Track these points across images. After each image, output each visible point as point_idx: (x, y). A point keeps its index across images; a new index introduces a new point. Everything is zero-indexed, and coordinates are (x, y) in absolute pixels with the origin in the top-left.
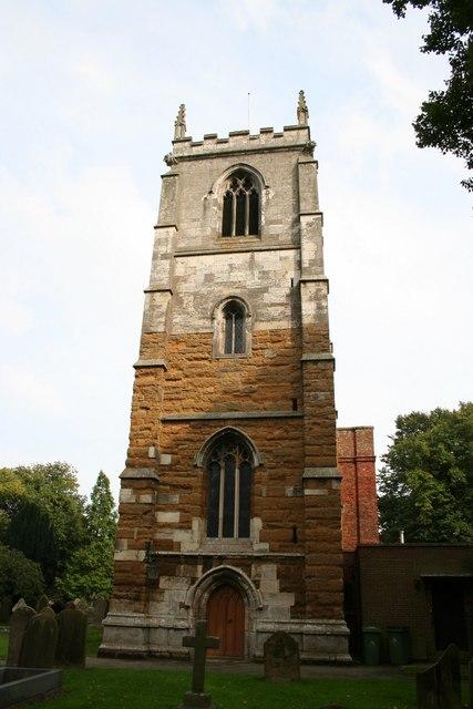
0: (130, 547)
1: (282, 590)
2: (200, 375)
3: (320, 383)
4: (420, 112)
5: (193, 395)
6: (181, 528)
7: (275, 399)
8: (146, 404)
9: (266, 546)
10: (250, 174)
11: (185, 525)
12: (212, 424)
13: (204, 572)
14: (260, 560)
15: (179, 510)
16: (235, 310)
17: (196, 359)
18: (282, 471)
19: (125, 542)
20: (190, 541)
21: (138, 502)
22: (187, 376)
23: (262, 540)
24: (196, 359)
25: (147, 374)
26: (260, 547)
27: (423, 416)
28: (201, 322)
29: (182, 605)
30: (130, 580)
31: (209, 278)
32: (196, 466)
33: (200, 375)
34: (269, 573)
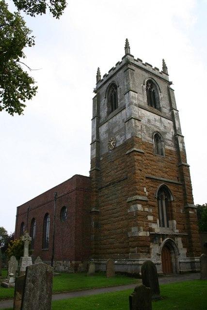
0: (144, 230)
1: (183, 247)
2: (151, 160)
3: (187, 174)
4: (27, 102)
5: (150, 168)
6: (154, 223)
7: (173, 176)
8: (140, 168)
9: (178, 231)
10: (154, 84)
11: (154, 222)
12: (158, 181)
13: (163, 240)
14: (177, 236)
15: (153, 215)
16: (158, 137)
17: (149, 153)
18: (179, 203)
19: (142, 228)
20: (157, 228)
21: (144, 211)
22: (147, 160)
23: (177, 229)
24: (149, 153)
25: (139, 155)
26: (177, 231)
27: (77, 178)
28: (149, 139)
29: (157, 254)
30: (145, 244)
31: (149, 121)
32: (155, 198)
33: (151, 160)
34: (179, 241)
